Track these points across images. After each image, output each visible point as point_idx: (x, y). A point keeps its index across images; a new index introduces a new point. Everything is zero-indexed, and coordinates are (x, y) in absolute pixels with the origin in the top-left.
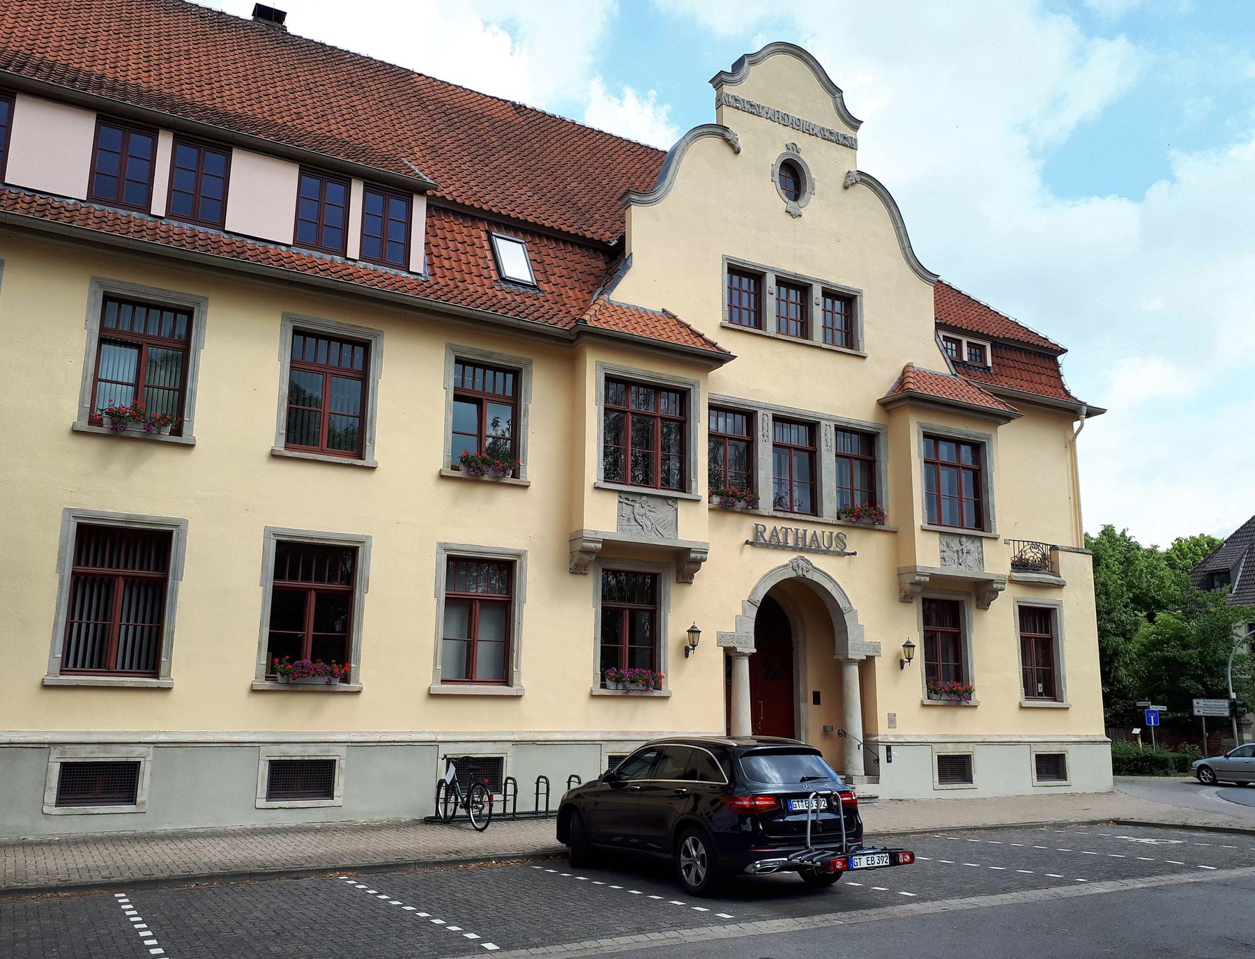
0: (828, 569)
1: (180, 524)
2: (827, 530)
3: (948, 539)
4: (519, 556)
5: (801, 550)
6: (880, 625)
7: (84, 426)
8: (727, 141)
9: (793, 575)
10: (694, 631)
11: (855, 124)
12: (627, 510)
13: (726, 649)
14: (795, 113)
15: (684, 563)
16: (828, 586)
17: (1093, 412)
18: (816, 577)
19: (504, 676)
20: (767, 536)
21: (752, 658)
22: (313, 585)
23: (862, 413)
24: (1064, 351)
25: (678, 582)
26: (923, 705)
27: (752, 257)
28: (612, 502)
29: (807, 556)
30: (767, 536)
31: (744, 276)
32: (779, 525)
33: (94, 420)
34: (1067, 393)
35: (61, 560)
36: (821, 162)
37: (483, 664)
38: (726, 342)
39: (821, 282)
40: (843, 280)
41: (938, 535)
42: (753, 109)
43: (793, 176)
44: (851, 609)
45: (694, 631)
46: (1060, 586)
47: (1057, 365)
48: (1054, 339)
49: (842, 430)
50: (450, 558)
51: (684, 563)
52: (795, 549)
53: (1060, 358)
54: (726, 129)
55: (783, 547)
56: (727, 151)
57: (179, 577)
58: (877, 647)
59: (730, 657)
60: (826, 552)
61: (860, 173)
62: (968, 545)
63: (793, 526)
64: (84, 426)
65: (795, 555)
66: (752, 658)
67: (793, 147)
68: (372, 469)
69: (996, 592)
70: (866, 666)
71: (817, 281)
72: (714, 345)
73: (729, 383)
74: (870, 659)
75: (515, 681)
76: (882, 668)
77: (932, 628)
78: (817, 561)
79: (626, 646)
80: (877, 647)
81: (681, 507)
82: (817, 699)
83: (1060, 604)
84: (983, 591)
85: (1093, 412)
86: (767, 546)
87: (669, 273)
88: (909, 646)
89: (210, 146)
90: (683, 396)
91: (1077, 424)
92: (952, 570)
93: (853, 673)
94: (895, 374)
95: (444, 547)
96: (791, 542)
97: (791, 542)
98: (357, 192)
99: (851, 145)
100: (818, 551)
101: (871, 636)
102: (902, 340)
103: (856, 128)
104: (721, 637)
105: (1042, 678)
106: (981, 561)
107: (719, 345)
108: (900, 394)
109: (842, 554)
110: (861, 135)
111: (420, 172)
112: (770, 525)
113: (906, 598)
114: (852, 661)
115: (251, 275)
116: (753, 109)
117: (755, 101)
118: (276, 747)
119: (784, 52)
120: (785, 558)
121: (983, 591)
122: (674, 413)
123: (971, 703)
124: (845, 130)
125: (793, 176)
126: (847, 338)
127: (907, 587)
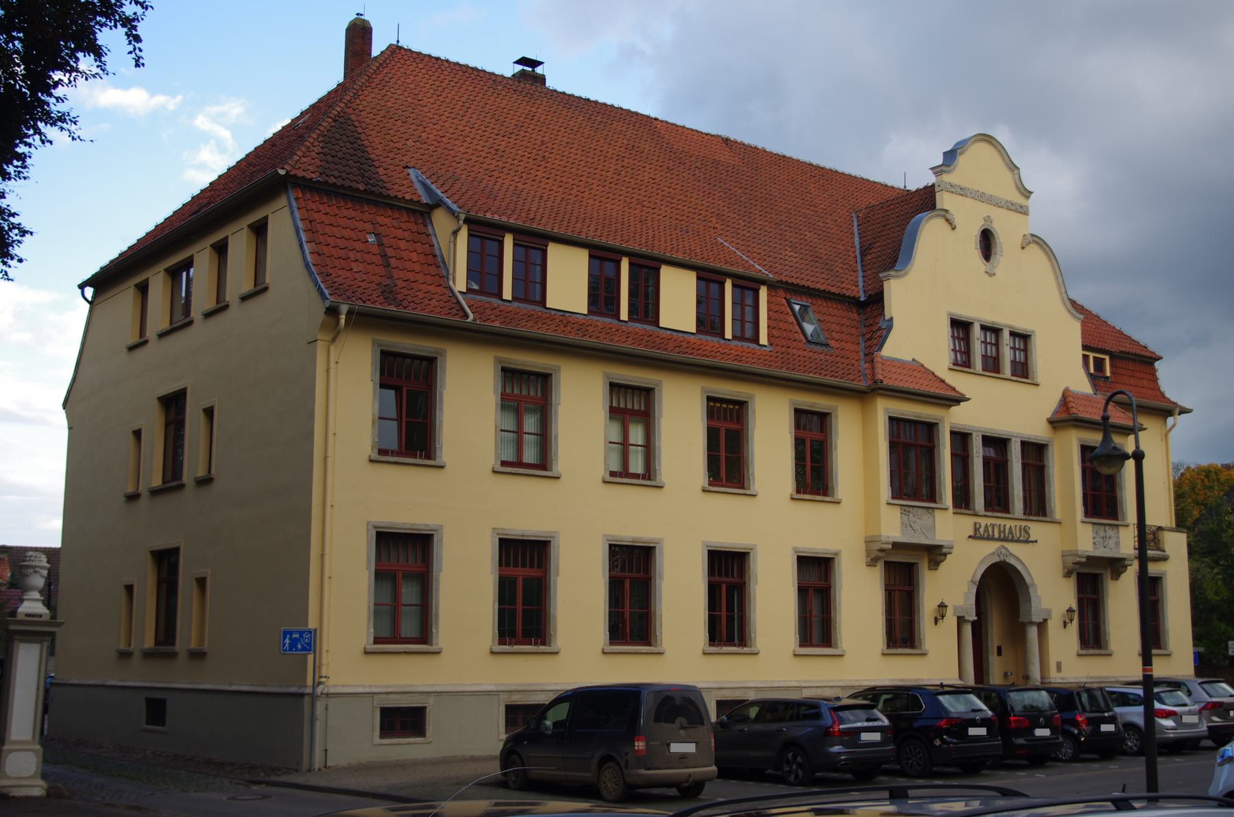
0: (1019, 554)
1: (439, 529)
2: (1018, 523)
3: (1097, 527)
4: (837, 554)
5: (1005, 540)
6: (1052, 595)
7: (375, 456)
8: (947, 220)
9: (998, 560)
10: (942, 606)
11: (1027, 194)
12: (905, 518)
13: (959, 618)
14: (989, 191)
15: (935, 554)
16: (1019, 567)
17: (1184, 411)
18: (1012, 561)
19: (424, 635)
20: (982, 530)
21: (974, 624)
22: (724, 579)
23: (1037, 430)
24: (1159, 358)
25: (1112, 578)
26: (1079, 655)
27: (964, 313)
28: (896, 512)
29: (1007, 545)
30: (982, 530)
31: (960, 327)
32: (989, 521)
33: (382, 452)
34: (1162, 394)
35: (368, 562)
36: (1008, 231)
37: (409, 627)
38: (960, 382)
39: (1010, 327)
40: (1022, 325)
41: (1090, 526)
42: (962, 192)
43: (987, 241)
44: (1034, 584)
45: (942, 606)
46: (1165, 559)
47: (1155, 370)
48: (1151, 348)
49: (1025, 444)
50: (799, 558)
51: (935, 554)
52: (999, 539)
53: (1157, 364)
54: (946, 211)
55: (990, 538)
56: (948, 227)
57: (661, 579)
58: (1049, 612)
59: (961, 620)
60: (1018, 541)
61: (1033, 235)
62: (1110, 532)
63: (997, 522)
64: (375, 456)
65: (998, 544)
66: (974, 624)
67: (988, 219)
68: (442, 467)
69: (1126, 567)
70: (1042, 626)
71: (1006, 326)
72: (954, 389)
73: (958, 417)
74: (1045, 621)
75: (434, 641)
76: (1054, 626)
77: (717, 579)
78: (1013, 548)
79: (520, 607)
80: (1049, 612)
81: (937, 513)
82: (999, 653)
83: (1165, 573)
84: (1116, 566)
85: (1184, 411)
86: (982, 538)
87: (915, 329)
88: (1070, 610)
89: (534, 244)
90: (930, 428)
91: (1170, 420)
92: (1101, 552)
93: (1033, 632)
94: (1057, 397)
95: (796, 550)
96: (996, 535)
97: (996, 535)
98: (508, 241)
99: (1024, 211)
100: (1012, 541)
101: (1045, 604)
102: (1062, 366)
103: (1028, 197)
104: (956, 608)
105: (1152, 636)
106: (1117, 544)
107: (957, 389)
108: (1064, 416)
109: (1027, 542)
110: (1031, 203)
111: (759, 269)
112: (983, 522)
113: (872, 562)
114: (1032, 623)
115: (679, 360)
116: (962, 192)
117: (964, 185)
118: (403, 696)
119: (981, 140)
120: (992, 547)
121: (1116, 566)
122: (922, 441)
123: (753, 650)
124: (1020, 200)
125: (987, 241)
126: (1022, 371)
127: (1071, 565)
